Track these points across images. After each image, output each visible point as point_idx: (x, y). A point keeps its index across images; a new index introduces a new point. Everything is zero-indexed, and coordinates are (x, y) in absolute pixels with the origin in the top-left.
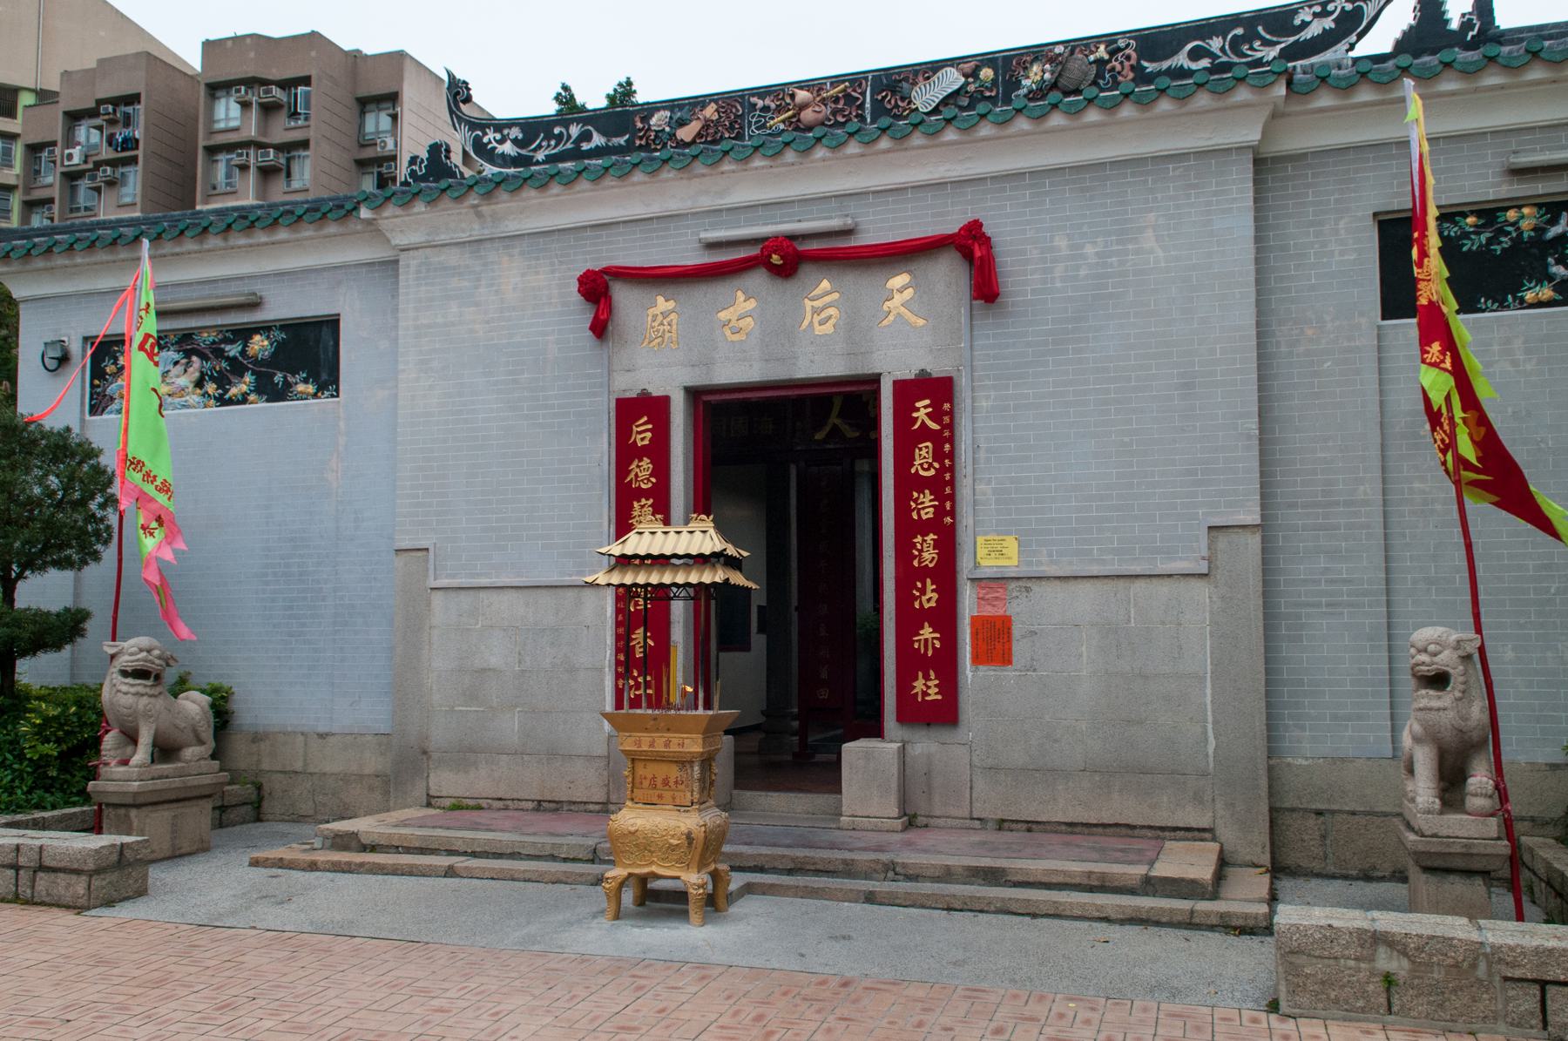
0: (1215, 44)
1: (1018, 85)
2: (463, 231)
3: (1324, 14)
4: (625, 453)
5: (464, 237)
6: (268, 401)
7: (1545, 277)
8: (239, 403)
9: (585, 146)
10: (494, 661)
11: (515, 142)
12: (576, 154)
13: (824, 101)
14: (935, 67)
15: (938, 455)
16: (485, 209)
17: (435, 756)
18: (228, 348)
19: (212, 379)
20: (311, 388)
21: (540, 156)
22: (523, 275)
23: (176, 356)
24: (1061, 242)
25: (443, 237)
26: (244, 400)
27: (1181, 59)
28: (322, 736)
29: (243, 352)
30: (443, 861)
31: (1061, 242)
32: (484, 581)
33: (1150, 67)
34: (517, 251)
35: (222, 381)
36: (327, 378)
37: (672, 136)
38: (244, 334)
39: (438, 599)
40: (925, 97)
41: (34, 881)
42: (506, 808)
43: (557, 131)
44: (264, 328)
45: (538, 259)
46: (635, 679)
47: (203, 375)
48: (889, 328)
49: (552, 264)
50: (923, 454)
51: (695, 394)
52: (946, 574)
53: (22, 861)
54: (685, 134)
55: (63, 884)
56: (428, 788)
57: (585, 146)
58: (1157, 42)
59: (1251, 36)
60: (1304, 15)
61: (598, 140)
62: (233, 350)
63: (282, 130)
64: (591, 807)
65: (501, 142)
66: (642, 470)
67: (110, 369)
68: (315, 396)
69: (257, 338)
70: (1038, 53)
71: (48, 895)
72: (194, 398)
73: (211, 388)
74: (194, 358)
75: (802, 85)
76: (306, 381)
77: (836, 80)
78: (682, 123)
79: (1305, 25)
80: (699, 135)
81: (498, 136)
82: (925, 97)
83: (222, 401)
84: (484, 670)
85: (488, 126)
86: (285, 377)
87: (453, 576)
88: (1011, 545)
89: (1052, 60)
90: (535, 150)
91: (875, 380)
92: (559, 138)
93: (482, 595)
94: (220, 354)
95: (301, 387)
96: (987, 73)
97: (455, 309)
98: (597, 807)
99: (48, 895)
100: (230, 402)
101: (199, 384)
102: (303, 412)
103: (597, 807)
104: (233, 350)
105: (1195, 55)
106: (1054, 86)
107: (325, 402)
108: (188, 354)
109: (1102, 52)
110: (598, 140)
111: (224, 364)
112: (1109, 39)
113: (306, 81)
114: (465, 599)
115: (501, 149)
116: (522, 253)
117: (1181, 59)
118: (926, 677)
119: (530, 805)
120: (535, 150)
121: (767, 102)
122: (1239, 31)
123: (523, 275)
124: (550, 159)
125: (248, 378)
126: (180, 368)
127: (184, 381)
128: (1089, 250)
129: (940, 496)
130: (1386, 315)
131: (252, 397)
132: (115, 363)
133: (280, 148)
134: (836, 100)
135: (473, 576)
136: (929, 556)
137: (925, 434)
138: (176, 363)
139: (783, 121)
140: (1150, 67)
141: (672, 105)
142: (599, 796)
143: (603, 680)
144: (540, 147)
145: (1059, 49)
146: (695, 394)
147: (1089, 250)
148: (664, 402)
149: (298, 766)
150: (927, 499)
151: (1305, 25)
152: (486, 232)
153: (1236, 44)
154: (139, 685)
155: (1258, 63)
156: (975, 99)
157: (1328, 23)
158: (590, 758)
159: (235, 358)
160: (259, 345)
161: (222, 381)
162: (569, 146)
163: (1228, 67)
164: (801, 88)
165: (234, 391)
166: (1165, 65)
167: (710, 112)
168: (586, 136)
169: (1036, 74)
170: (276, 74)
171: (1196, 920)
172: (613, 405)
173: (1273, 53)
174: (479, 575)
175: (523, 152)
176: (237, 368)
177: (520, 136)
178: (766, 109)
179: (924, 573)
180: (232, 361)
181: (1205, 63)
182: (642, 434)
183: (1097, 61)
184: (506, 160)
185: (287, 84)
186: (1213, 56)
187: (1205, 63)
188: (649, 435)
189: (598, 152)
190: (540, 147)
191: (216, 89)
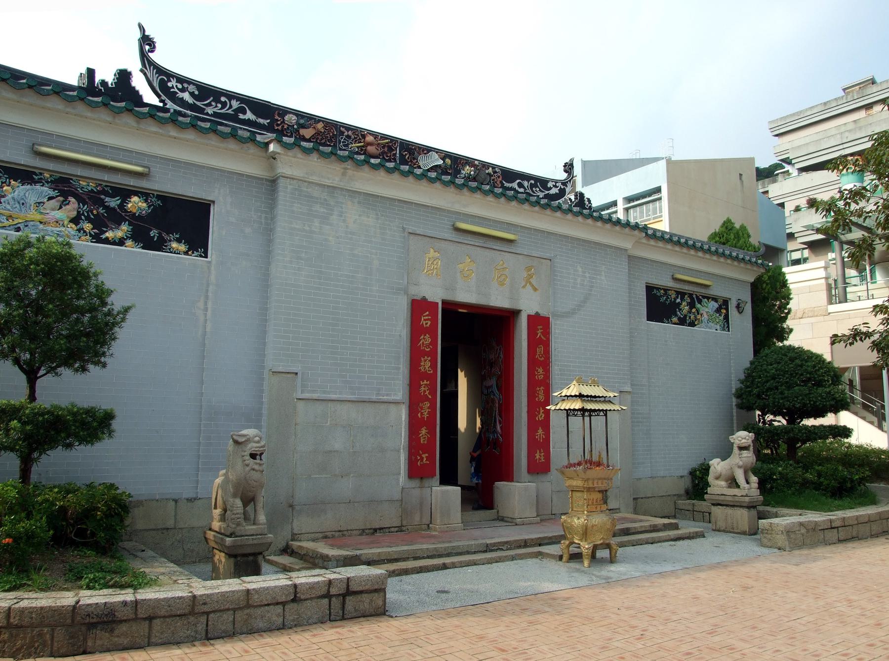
0: (526, 184)
1: (459, 173)
2: (329, 179)
3: (555, 186)
5: (328, 182)
6: (143, 248)
7: (676, 315)
8: (114, 243)
9: (241, 116)
10: (337, 446)
11: (192, 94)
14: (427, 150)
16: (350, 172)
17: (297, 508)
18: (107, 199)
19: (88, 219)
20: (183, 247)
21: (210, 110)
22: (360, 216)
23: (53, 193)
25: (314, 179)
26: (121, 242)
27: (515, 185)
28: (189, 500)
29: (122, 206)
32: (333, 397)
33: (507, 185)
34: (356, 200)
36: (197, 241)
38: (125, 194)
39: (301, 405)
42: (343, 535)
43: (223, 99)
44: (144, 195)
45: (369, 209)
46: (420, 456)
49: (377, 214)
50: (540, 350)
51: (444, 302)
54: (307, 133)
55: (368, 601)
56: (292, 529)
57: (241, 116)
58: (509, 175)
61: (249, 115)
62: (113, 203)
64: (392, 529)
65: (183, 90)
68: (186, 253)
69: (135, 199)
70: (469, 161)
71: (356, 610)
73: (88, 226)
74: (72, 199)
75: (371, 133)
76: (179, 241)
77: (384, 137)
78: (303, 126)
79: (551, 188)
81: (180, 86)
84: (330, 451)
85: (173, 77)
86: (160, 234)
87: (313, 392)
90: (207, 105)
92: (224, 105)
93: (330, 404)
94: (102, 203)
95: (174, 245)
97: (317, 224)
98: (396, 529)
99: (356, 610)
100: (107, 241)
101: (75, 221)
102: (175, 259)
103: (396, 529)
104: (113, 203)
107: (194, 259)
108: (65, 194)
110: (249, 115)
111: (101, 210)
112: (494, 166)
114: (319, 408)
116: (359, 203)
117: (515, 185)
119: (357, 532)
120: (207, 105)
122: (533, 182)
123: (360, 216)
124: (215, 114)
125: (125, 227)
131: (129, 243)
135: (325, 392)
138: (50, 199)
139: (358, 147)
141: (299, 114)
142: (397, 523)
143: (399, 457)
144: (209, 105)
146: (444, 302)
149: (170, 523)
152: (342, 184)
153: (532, 186)
158: (391, 501)
159: (114, 209)
160: (136, 204)
162: (230, 111)
164: (372, 135)
165: (109, 234)
167: (320, 126)
169: (468, 170)
171: (847, 524)
172: (410, 301)
174: (329, 393)
175: (198, 103)
177: (197, 93)
178: (349, 137)
182: (425, 322)
183: (488, 174)
188: (429, 323)
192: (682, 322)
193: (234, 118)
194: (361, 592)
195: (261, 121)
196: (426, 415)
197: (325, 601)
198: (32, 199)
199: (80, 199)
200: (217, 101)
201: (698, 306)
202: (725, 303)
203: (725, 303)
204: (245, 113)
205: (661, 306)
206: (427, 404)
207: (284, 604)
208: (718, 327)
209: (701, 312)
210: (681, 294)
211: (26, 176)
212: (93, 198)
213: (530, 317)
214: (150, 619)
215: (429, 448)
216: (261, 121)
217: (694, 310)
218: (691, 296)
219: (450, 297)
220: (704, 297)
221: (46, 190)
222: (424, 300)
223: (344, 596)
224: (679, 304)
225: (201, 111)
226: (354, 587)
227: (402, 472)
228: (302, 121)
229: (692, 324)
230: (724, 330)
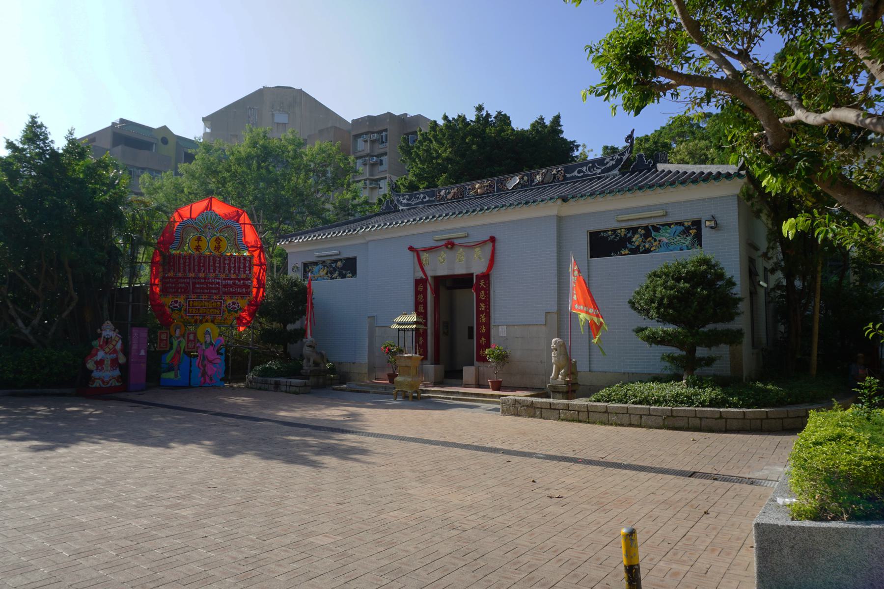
0: (584, 169)
3: (613, 160)
4: (417, 293)
7: (626, 247)
12: (423, 203)
15: (486, 294)
27: (576, 173)
33: (568, 175)
36: (354, 273)
38: (336, 261)
44: (341, 260)
48: (471, 263)
54: (449, 197)
59: (593, 166)
60: (608, 160)
62: (334, 265)
63: (379, 149)
66: (421, 297)
78: (449, 193)
83: (332, 278)
91: (472, 274)
102: (349, 281)
105: (579, 172)
107: (354, 278)
110: (427, 198)
113: (386, 130)
117: (576, 173)
129: (486, 304)
133: (377, 156)
136: (484, 320)
137: (483, 289)
140: (568, 175)
154: (311, 349)
155: (595, 174)
156: (523, 186)
157: (614, 162)
160: (339, 264)
161: (332, 274)
163: (588, 175)
168: (424, 198)
170: (376, 129)
173: (599, 171)
176: (335, 270)
182: (421, 288)
185: (380, 132)
186: (583, 172)
189: (427, 202)
191: (357, 137)
192: (635, 251)
202: (697, 224)
203: (697, 224)
210: (628, 229)
218: (646, 228)
220: (663, 225)
224: (631, 238)
225: (410, 205)
229: (648, 251)
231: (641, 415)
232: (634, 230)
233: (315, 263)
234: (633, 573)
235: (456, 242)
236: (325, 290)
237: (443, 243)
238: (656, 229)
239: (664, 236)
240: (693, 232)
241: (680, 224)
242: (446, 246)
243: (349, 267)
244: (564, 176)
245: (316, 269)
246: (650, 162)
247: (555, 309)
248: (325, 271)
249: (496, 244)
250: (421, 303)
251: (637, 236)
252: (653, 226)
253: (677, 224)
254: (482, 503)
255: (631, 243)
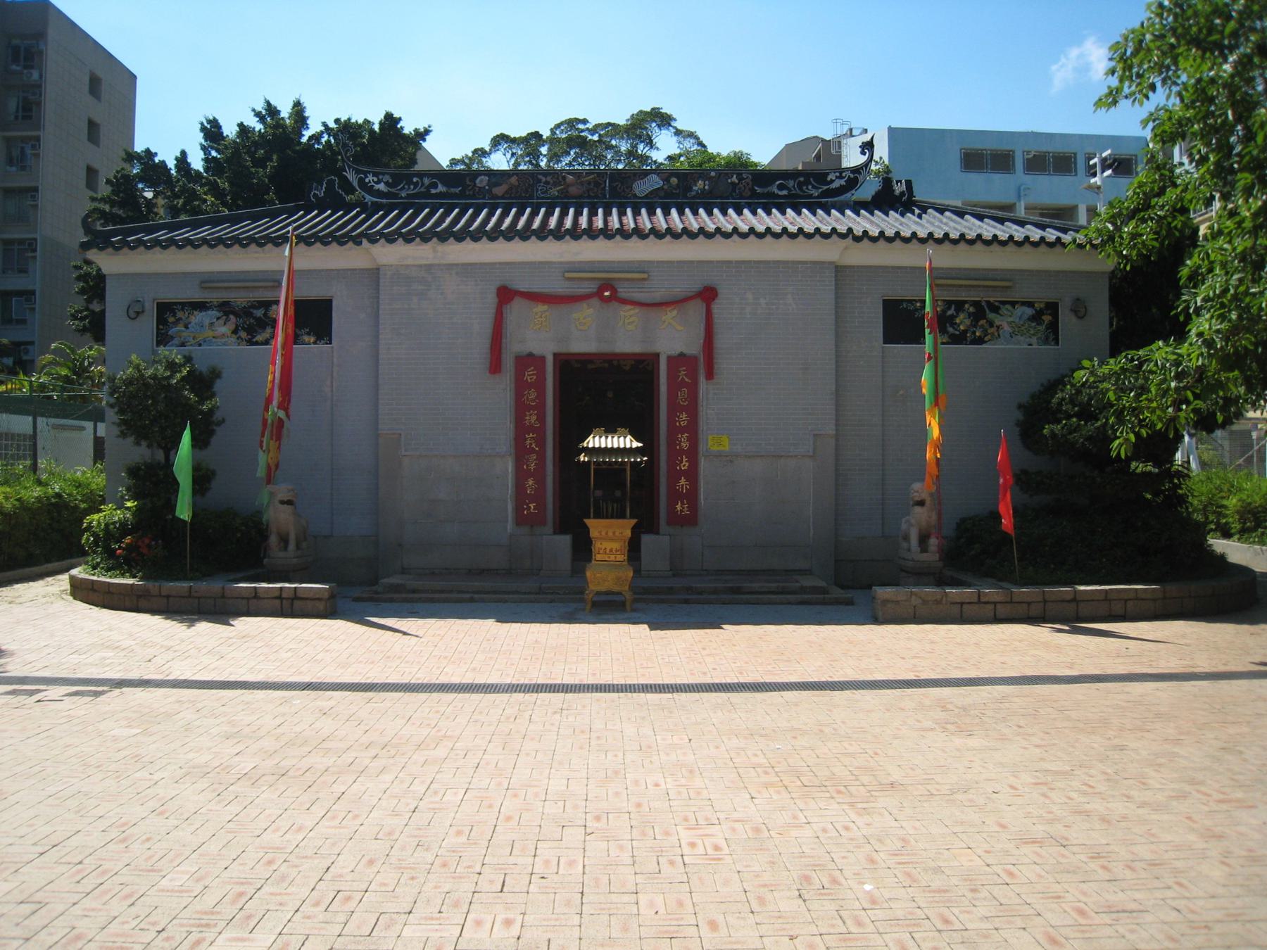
0: (791, 183)
1: (690, 189)
3: (841, 177)
8: (262, 344)
9: (433, 191)
11: (387, 184)
13: (582, 184)
19: (243, 329)
23: (219, 314)
24: (750, 296)
29: (265, 315)
30: (468, 596)
31: (750, 296)
35: (251, 331)
37: (490, 191)
40: (642, 188)
41: (292, 604)
43: (415, 180)
47: (237, 326)
50: (683, 394)
51: (555, 355)
52: (693, 453)
53: (284, 595)
54: (499, 191)
57: (433, 191)
59: (807, 183)
60: (831, 177)
61: (441, 188)
62: (259, 313)
67: (171, 319)
68: (315, 343)
72: (233, 339)
73: (243, 334)
74: (232, 317)
76: (308, 334)
79: (832, 181)
80: (506, 192)
82: (642, 188)
83: (251, 342)
88: (725, 440)
89: (710, 179)
91: (657, 355)
92: (416, 185)
94: (250, 315)
95: (306, 338)
96: (674, 180)
100: (257, 343)
101: (235, 332)
104: (259, 313)
105: (781, 187)
106: (710, 192)
107: (322, 346)
108: (227, 314)
109: (735, 179)
110: (441, 188)
115: (377, 187)
118: (683, 504)
121: (549, 179)
124: (409, 196)
126: (221, 321)
127: (225, 330)
128: (762, 301)
130: (888, 339)
132: (174, 315)
134: (589, 183)
136: (685, 465)
140: (759, 190)
144: (403, 188)
145: (713, 174)
146: (555, 355)
147: (762, 301)
148: (542, 359)
150: (684, 416)
151: (832, 181)
153: (800, 185)
155: (811, 196)
157: (843, 182)
161: (251, 331)
165: (259, 338)
166: (766, 190)
179: (682, 452)
180: (258, 319)
181: (785, 192)
182: (530, 376)
183: (733, 183)
184: (379, 194)
187: (785, 192)
190: (403, 188)
193: (427, 195)
194: (307, 599)
195: (452, 190)
196: (533, 466)
197: (278, 602)
198: (207, 322)
199: (237, 315)
200: (410, 182)
201: (991, 316)
202: (1053, 308)
203: (1053, 308)
204: (436, 187)
205: (901, 322)
206: (534, 456)
207: (248, 599)
208: (1034, 340)
209: (997, 323)
211: (201, 306)
212: (246, 312)
213: (670, 358)
214: (168, 597)
215: (539, 497)
216: (452, 190)
217: (982, 322)
218: (976, 304)
219: (563, 350)
220: (1004, 303)
221: (215, 313)
222: (530, 355)
223: (293, 599)
224: (953, 317)
225: (395, 196)
226: (300, 594)
227: (510, 519)
228: (494, 180)
229: (980, 341)
230: (1046, 342)
231: (1126, 601)
232: (960, 305)
233: (201, 306)
234: (26, 685)
235: (623, 292)
236: (250, 371)
237: (590, 288)
238: (995, 308)
239: (1004, 321)
240: (1047, 318)
241: (1030, 304)
242: (598, 294)
243: (314, 318)
244: (753, 191)
245: (198, 317)
246: (331, 183)
247: (831, 430)
248: (231, 326)
249: (716, 308)
250: (530, 408)
251: (962, 316)
252: (988, 302)
253: (1023, 303)
254: (1143, 840)
255: (953, 325)
